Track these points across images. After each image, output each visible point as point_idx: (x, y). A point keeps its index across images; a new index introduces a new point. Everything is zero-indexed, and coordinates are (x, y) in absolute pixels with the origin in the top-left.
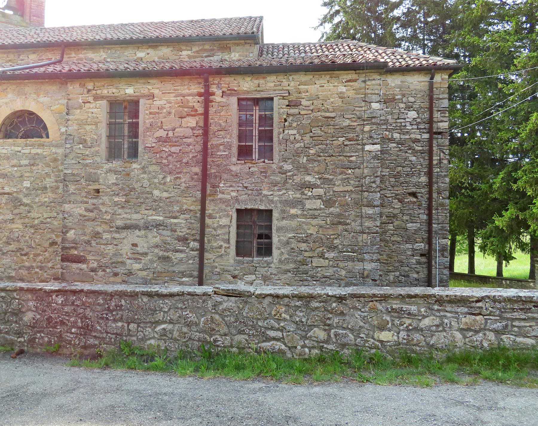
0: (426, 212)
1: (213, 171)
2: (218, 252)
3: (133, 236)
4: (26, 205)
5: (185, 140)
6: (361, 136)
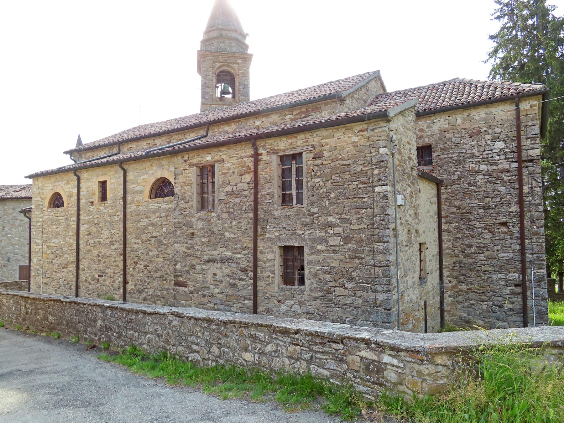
0: (519, 242)
1: (262, 216)
2: (267, 281)
3: (213, 268)
4: (165, 245)
5: (244, 193)
6: (371, 179)
